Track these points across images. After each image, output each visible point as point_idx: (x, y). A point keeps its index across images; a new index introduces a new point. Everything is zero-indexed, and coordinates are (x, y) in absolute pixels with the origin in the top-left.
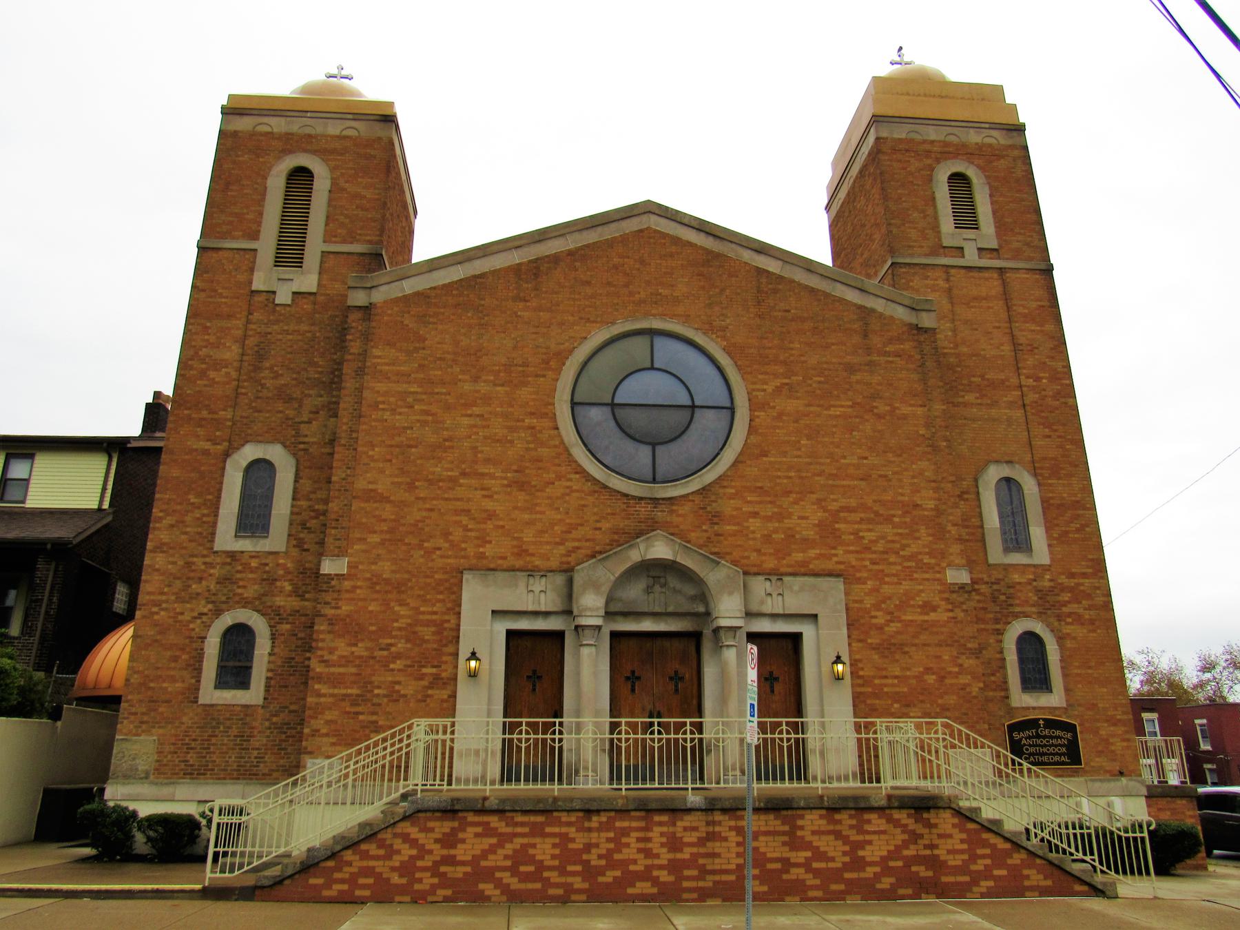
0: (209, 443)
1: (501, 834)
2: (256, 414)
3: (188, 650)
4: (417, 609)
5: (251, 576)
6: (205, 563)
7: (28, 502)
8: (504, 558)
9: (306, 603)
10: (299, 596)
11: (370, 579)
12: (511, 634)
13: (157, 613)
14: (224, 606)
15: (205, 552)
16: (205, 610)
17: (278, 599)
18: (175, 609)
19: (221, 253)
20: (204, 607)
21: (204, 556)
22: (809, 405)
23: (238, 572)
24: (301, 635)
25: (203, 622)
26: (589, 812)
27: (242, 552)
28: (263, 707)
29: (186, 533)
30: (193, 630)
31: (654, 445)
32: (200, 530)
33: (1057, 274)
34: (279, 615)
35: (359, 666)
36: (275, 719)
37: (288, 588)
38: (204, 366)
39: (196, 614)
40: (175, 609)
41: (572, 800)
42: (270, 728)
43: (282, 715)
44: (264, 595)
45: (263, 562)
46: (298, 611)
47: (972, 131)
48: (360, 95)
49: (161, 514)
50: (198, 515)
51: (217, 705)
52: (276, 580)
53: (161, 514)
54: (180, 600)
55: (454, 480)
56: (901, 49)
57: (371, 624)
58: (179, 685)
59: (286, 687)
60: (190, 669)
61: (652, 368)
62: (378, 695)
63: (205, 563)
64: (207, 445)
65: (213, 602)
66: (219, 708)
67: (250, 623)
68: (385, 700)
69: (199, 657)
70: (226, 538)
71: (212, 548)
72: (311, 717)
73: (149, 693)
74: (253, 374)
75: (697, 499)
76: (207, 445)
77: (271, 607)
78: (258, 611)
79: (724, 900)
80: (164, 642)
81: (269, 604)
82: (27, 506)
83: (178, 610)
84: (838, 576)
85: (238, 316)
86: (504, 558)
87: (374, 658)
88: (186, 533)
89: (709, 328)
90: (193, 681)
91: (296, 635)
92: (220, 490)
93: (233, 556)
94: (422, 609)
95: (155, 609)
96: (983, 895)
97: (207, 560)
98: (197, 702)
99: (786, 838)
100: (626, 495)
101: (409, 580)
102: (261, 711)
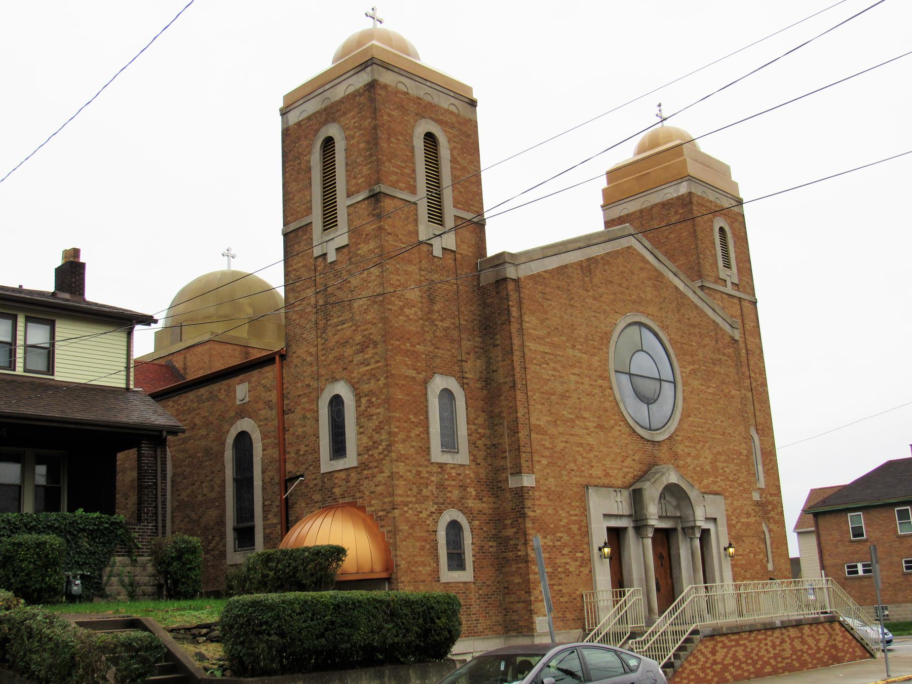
0: (415, 372)
1: (728, 647)
2: (436, 350)
3: (429, 541)
4: (568, 512)
5: (453, 483)
6: (427, 472)
7: (56, 374)
8: (600, 478)
9: (484, 505)
10: (479, 499)
11: (546, 491)
12: (610, 530)
13: (407, 512)
14: (443, 507)
15: (426, 463)
16: (433, 510)
17: (469, 501)
18: (416, 509)
19: (395, 200)
20: (433, 507)
21: (427, 466)
22: (702, 385)
23: (446, 480)
24: (485, 529)
25: (434, 519)
26: (751, 632)
27: (446, 464)
28: (474, 583)
29: (413, 447)
30: (429, 525)
31: (648, 404)
32: (421, 444)
33: (759, 305)
34: (472, 514)
35: (549, 552)
36: (480, 592)
37: (474, 493)
38: (401, 304)
39: (429, 513)
40: (416, 509)
41: (745, 626)
42: (479, 598)
43: (483, 588)
44: (462, 498)
45: (458, 472)
46: (481, 511)
47: (725, 198)
48: (417, 56)
49: (396, 430)
50: (418, 433)
51: (450, 583)
52: (467, 487)
53: (396, 430)
54: (419, 502)
55: (572, 420)
56: (660, 105)
57: (552, 523)
58: (428, 568)
59: (483, 568)
60: (432, 555)
61: (642, 350)
62: (560, 572)
63: (427, 472)
64: (412, 373)
65: (437, 503)
66: (452, 585)
67: (459, 520)
68: (564, 575)
69: (435, 548)
70: (437, 455)
71: (429, 460)
72: (533, 589)
73: (413, 575)
74: (429, 316)
75: (668, 442)
76: (412, 373)
77: (467, 508)
78: (461, 511)
79: (789, 672)
80: (415, 535)
81: (466, 505)
82: (57, 378)
83: (419, 510)
84: (720, 494)
85: (414, 262)
86: (600, 478)
87: (555, 546)
88: (413, 447)
89: (664, 328)
90: (435, 565)
91: (482, 529)
92: (427, 412)
93: (441, 466)
94: (571, 512)
95: (406, 509)
96: (848, 661)
97: (429, 469)
98: (439, 581)
99: (800, 640)
100: (642, 438)
101: (563, 492)
102: (473, 586)
